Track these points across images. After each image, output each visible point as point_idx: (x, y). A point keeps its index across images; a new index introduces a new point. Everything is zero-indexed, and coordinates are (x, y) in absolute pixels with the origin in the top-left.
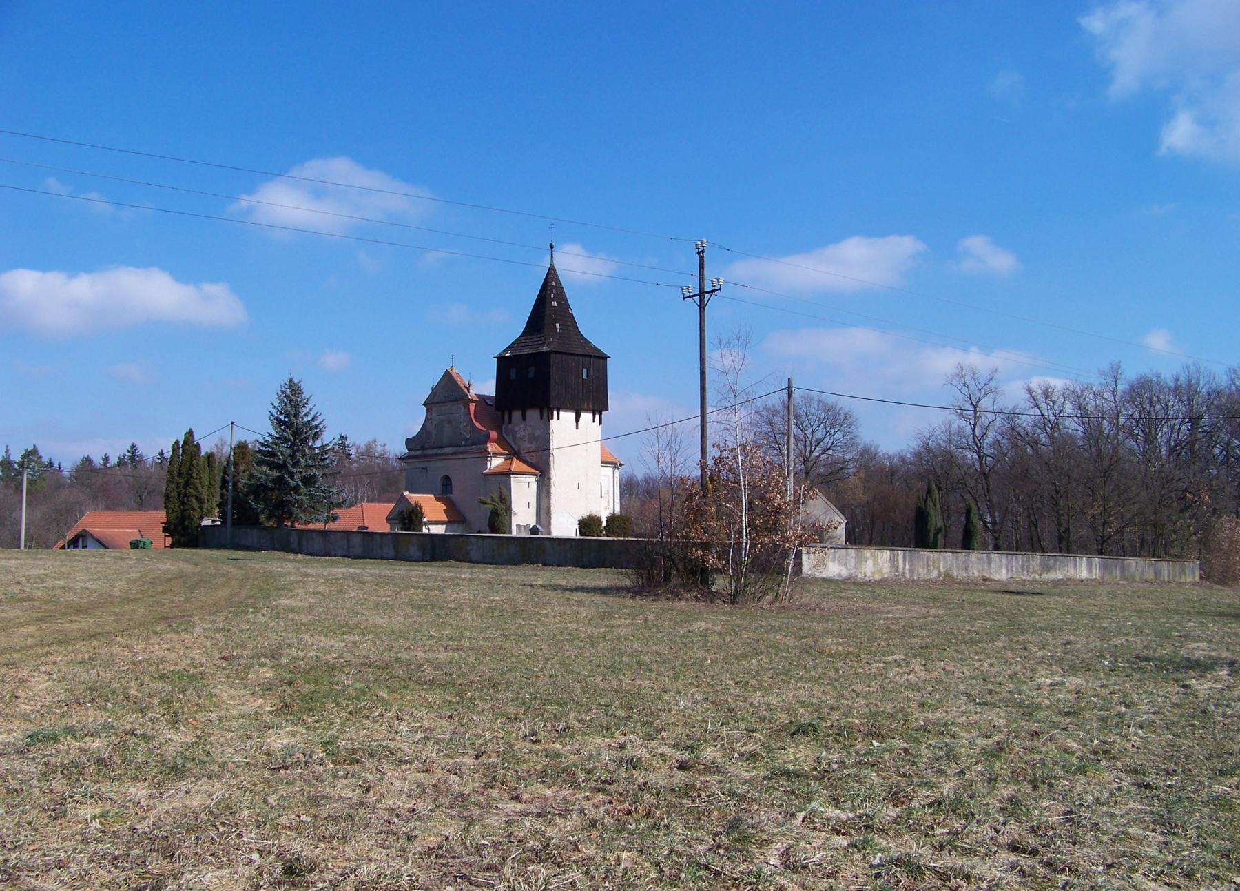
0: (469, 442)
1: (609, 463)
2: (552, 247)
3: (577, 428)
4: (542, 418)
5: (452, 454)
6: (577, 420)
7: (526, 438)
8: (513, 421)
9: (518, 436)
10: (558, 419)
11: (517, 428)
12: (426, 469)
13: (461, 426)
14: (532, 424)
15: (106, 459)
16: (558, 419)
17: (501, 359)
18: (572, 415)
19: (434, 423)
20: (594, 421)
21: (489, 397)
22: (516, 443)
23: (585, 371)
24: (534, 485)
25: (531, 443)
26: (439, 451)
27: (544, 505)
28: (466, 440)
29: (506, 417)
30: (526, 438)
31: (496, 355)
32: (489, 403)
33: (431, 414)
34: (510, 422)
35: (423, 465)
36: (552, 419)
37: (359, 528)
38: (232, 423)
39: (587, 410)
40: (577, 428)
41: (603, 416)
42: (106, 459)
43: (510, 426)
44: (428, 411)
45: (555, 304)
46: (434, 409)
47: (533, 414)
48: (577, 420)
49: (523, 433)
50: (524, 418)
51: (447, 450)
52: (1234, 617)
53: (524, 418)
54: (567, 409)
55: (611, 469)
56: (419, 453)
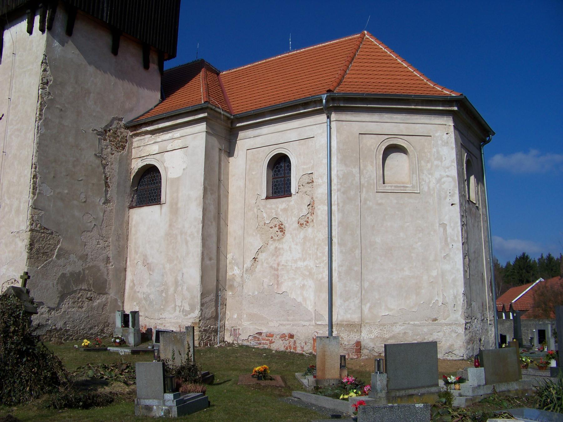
1: (305, 105)
55: (323, 118)
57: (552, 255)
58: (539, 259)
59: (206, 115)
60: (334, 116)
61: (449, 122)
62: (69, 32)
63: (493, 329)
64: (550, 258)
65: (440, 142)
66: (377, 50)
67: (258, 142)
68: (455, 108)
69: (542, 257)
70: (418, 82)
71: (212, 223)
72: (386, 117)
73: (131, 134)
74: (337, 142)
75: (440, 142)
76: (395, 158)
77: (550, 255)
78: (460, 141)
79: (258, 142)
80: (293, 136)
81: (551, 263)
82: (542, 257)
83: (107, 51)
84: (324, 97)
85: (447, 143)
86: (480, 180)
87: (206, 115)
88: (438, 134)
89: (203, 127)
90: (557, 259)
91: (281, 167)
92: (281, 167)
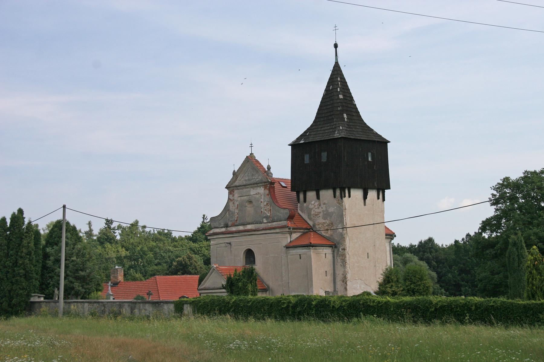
0: (271, 219)
2: (336, 46)
3: (365, 204)
4: (335, 197)
5: (254, 231)
6: (365, 197)
7: (321, 215)
8: (307, 199)
9: (313, 212)
10: (349, 196)
11: (311, 206)
12: (230, 243)
13: (262, 205)
14: (326, 201)
15: (442, 245)
16: (349, 196)
17: (295, 146)
19: (237, 203)
20: (378, 198)
21: (284, 180)
22: (310, 219)
23: (370, 154)
24: (330, 257)
25: (325, 218)
26: (241, 228)
27: (339, 272)
28: (267, 218)
29: (301, 196)
30: (321, 215)
31: (290, 142)
32: (284, 185)
33: (233, 196)
34: (305, 201)
35: (227, 240)
36: (345, 197)
37: (180, 298)
38: (64, 207)
39: (373, 188)
40: (365, 204)
41: (307, 197)
42: (442, 245)
43: (305, 205)
44: (230, 193)
45: (341, 97)
46: (236, 191)
47: (327, 194)
48: (365, 197)
49: (317, 210)
50: (318, 197)
51: (249, 227)
52: (152, 303)
53: (318, 197)
54: (356, 187)
56: (223, 230)
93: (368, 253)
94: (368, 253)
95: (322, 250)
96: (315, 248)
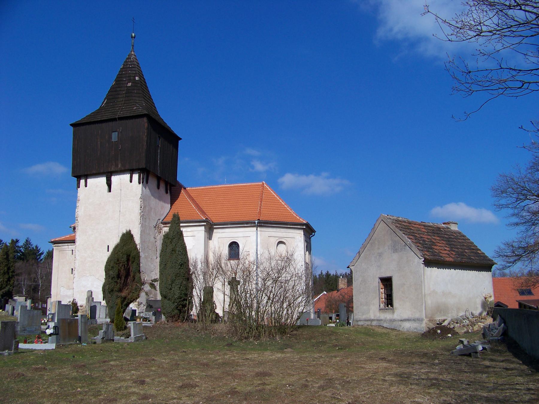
1: (247, 223)
18: (103, 180)
55: (255, 229)
57: (330, 272)
58: (319, 275)
59: (205, 224)
60: (259, 229)
61: (301, 232)
62: (147, 182)
63: (451, 259)
64: (328, 275)
65: (298, 240)
66: (274, 199)
67: (224, 235)
68: (305, 227)
69: (322, 273)
70: (290, 213)
71: (157, 258)
72: (278, 229)
73: (163, 226)
74: (260, 240)
75: (298, 240)
76: (281, 246)
77: (328, 272)
78: (305, 239)
79: (224, 235)
80: (241, 235)
81: (329, 279)
82: (322, 273)
83: (156, 187)
84: (256, 222)
85: (300, 241)
86: (310, 253)
87: (205, 224)
88: (297, 237)
89: (203, 228)
90: (333, 275)
91: (233, 247)
92: (233, 247)
93: (108, 246)
94: (108, 246)
95: (67, 247)
96: (57, 245)
